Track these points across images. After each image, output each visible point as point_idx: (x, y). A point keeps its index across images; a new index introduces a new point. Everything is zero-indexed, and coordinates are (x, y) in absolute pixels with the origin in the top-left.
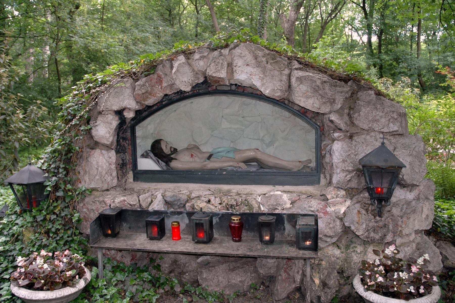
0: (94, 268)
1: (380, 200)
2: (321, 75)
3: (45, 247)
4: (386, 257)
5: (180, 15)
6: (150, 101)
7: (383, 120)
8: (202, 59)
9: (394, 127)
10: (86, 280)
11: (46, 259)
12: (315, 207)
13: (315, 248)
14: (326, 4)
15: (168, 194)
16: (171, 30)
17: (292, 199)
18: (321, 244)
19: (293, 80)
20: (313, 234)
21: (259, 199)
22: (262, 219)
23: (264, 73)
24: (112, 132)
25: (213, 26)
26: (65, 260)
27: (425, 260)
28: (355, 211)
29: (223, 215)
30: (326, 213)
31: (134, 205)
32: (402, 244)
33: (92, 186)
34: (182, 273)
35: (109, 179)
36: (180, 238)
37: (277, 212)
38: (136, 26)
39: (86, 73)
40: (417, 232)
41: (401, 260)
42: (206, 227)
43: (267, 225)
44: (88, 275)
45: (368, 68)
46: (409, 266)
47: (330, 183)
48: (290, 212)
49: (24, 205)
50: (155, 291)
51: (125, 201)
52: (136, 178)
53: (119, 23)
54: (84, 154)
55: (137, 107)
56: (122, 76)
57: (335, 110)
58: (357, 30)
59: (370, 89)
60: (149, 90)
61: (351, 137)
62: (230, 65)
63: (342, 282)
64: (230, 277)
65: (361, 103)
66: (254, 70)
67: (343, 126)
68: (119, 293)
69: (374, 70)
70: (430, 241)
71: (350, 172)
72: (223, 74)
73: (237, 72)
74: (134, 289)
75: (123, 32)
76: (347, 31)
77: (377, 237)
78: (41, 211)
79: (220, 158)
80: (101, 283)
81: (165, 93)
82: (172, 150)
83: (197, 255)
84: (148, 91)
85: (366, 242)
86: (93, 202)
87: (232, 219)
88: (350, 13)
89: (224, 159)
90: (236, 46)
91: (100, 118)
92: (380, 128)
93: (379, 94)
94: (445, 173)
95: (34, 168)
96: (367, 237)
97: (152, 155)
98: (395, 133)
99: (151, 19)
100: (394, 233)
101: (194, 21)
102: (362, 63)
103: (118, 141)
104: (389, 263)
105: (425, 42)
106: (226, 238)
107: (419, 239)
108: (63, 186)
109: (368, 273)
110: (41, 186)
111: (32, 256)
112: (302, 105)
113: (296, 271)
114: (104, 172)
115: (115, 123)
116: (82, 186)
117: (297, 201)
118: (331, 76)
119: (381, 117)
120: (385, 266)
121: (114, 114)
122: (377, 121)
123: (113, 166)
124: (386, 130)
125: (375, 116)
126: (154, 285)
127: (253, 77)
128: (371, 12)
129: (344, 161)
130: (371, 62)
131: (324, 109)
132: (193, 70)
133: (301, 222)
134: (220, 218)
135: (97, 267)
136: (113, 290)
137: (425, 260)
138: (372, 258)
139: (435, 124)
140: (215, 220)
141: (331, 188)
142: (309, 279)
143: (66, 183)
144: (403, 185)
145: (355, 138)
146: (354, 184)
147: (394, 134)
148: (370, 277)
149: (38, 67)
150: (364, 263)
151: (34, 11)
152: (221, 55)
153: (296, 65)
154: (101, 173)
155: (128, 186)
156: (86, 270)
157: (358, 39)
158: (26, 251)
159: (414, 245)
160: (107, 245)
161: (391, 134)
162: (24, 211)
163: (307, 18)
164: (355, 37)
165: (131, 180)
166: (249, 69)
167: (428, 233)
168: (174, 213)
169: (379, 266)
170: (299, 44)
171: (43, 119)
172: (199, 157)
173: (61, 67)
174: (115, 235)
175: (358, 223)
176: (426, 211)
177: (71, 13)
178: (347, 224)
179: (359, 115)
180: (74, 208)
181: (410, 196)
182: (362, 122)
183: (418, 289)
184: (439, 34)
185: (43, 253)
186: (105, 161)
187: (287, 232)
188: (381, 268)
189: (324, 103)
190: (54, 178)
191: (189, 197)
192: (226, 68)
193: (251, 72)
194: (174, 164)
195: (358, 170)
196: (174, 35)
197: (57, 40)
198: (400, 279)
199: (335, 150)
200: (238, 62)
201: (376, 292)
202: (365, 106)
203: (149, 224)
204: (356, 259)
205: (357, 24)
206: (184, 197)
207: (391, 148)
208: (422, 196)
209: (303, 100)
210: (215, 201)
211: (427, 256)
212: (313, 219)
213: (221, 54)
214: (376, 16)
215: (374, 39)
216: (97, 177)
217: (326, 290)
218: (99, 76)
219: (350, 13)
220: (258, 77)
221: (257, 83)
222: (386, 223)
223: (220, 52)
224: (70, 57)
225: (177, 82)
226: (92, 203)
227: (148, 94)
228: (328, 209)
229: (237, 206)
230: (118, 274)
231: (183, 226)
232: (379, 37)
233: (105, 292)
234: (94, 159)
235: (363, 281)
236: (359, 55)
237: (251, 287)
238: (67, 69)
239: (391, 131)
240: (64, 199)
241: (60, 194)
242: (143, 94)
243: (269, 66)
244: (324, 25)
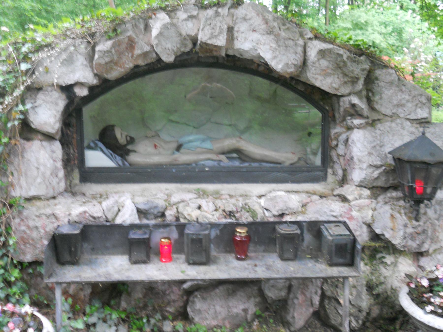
6: (113, 75)
7: (410, 105)
8: (190, 19)
12: (338, 211)
17: (302, 201)
20: (349, 247)
23: (277, 42)
29: (226, 226)
31: (99, 218)
33: (33, 193)
35: (54, 181)
51: (85, 212)
55: (94, 81)
57: (355, 91)
60: (115, 58)
62: (230, 30)
64: (231, 304)
65: (382, 84)
71: (377, 167)
72: (221, 41)
73: (239, 39)
79: (193, 149)
81: (136, 63)
82: (128, 138)
84: (114, 59)
86: (36, 216)
87: (237, 232)
89: (199, 150)
92: (406, 114)
96: (404, 247)
97: (100, 145)
98: (423, 120)
113: (314, 291)
114: (48, 173)
117: (308, 203)
119: (408, 101)
121: (59, 90)
122: (403, 105)
123: (59, 164)
124: (413, 117)
125: (401, 100)
127: (262, 47)
129: (370, 154)
134: (221, 231)
146: (380, 183)
152: (218, 16)
154: (43, 175)
161: (418, 121)
166: (256, 36)
172: (164, 148)
174: (74, 262)
175: (392, 229)
178: (378, 231)
179: (381, 98)
186: (47, 155)
189: (346, 83)
192: (225, 34)
193: (259, 40)
194: (133, 158)
199: (355, 140)
202: (386, 87)
209: (320, 78)
213: (217, 14)
216: (39, 180)
220: (268, 47)
222: (426, 228)
223: (217, 12)
226: (35, 218)
227: (112, 63)
229: (237, 212)
234: (32, 154)
239: (419, 118)
242: (106, 63)
243: (283, 34)
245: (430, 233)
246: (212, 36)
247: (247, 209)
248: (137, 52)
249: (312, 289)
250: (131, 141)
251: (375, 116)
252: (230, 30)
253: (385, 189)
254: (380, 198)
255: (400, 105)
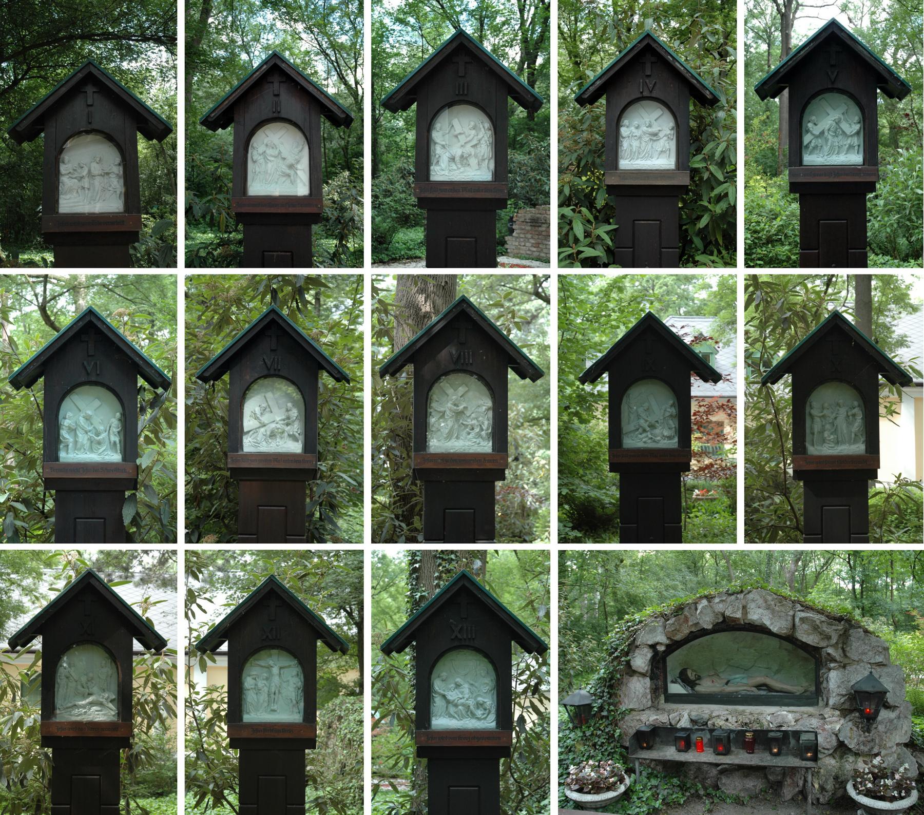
0: (633, 775)
1: (868, 719)
2: (820, 616)
3: (590, 757)
4: (874, 766)
5: (703, 567)
6: (678, 637)
7: (870, 653)
9: (879, 659)
10: (625, 785)
11: (593, 768)
13: (815, 759)
14: (819, 559)
15: (694, 714)
16: (695, 579)
18: (820, 756)
19: (797, 620)
21: (769, 718)
22: (771, 735)
24: (647, 662)
25: (729, 576)
26: (608, 769)
27: (905, 769)
28: (848, 728)
29: (739, 732)
30: (824, 730)
32: (886, 755)
33: (631, 707)
34: (705, 779)
35: (645, 701)
36: (703, 751)
37: (783, 729)
38: (668, 576)
39: (628, 614)
40: (898, 745)
41: (885, 768)
42: (725, 741)
43: (775, 740)
44: (628, 781)
45: (854, 608)
46: (893, 774)
47: (827, 704)
48: (794, 729)
49: (576, 722)
50: (683, 794)
52: (667, 701)
53: (654, 573)
54: (625, 680)
55: (668, 642)
56: (656, 616)
58: (843, 579)
59: (860, 627)
61: (844, 667)
62: (744, 607)
63: (837, 786)
66: (766, 612)
67: (838, 658)
68: (653, 796)
69: (858, 611)
70: (908, 752)
71: (843, 696)
72: (738, 615)
74: (665, 793)
75: (657, 580)
76: (836, 580)
77: (866, 749)
78: (589, 727)
80: (638, 787)
83: (717, 765)
85: (857, 754)
88: (838, 567)
90: (749, 592)
91: (637, 651)
93: (866, 631)
94: (916, 694)
95: (583, 692)
97: (679, 680)
99: (680, 570)
100: (880, 746)
101: (714, 571)
102: (848, 605)
103: (652, 670)
104: (876, 771)
105: (897, 589)
106: (741, 751)
107: (899, 750)
108: (607, 707)
109: (859, 780)
110: (589, 707)
111: (582, 765)
112: (804, 640)
115: (649, 655)
116: (623, 708)
118: (827, 616)
120: (873, 774)
122: (865, 654)
123: (648, 691)
126: (682, 789)
128: (854, 565)
129: (839, 687)
130: (854, 604)
131: (823, 644)
132: (649, 708)
133: (804, 737)
135: (635, 773)
136: (648, 793)
137: (905, 769)
138: (861, 766)
139: (909, 654)
140: (732, 736)
141: (828, 709)
142: (810, 785)
143: (609, 704)
144: (887, 707)
145: (848, 668)
146: (846, 706)
147: (880, 664)
148: (861, 783)
149: (590, 608)
150: (856, 771)
151: (588, 565)
153: (799, 607)
155: (660, 706)
156: (626, 777)
157: (844, 586)
158: (577, 760)
159: (896, 756)
160: (643, 756)
162: (575, 728)
163: (804, 570)
164: (842, 585)
165: (663, 701)
166: (760, 611)
167: (906, 745)
168: (697, 730)
169: (868, 774)
170: (798, 591)
171: (593, 650)
173: (608, 609)
174: (649, 748)
176: (905, 728)
177: (617, 566)
178: (841, 739)
180: (616, 725)
181: (892, 715)
182: (853, 655)
183: (900, 793)
184: (908, 583)
185: (591, 762)
187: (791, 745)
188: (870, 776)
190: (600, 701)
191: (710, 716)
194: (698, 688)
195: (850, 694)
196: (699, 583)
197: (605, 587)
198: (885, 785)
200: (752, 605)
201: (865, 795)
203: (677, 739)
204: (848, 767)
205: (843, 574)
206: (707, 716)
207: (877, 676)
208: (902, 715)
210: (732, 720)
211: (907, 765)
212: (813, 735)
213: (737, 599)
214: (859, 569)
215: (857, 586)
217: (824, 793)
218: (637, 617)
219: (838, 567)
221: (767, 623)
224: (616, 601)
225: (701, 622)
227: (677, 631)
228: (826, 727)
230: (652, 780)
231: (705, 740)
232: (861, 586)
233: (641, 794)
235: (854, 786)
236: (846, 599)
237: (761, 790)
238: (613, 610)
240: (607, 717)
241: (605, 713)
243: (777, 608)
244: (818, 575)
245: (877, 741)
246: (734, 612)
247: (758, 721)
248: (690, 623)
249: (798, 776)
250: (699, 678)
251: (846, 661)
252: (744, 607)
253: (851, 711)
254: (847, 718)
255: (864, 653)
